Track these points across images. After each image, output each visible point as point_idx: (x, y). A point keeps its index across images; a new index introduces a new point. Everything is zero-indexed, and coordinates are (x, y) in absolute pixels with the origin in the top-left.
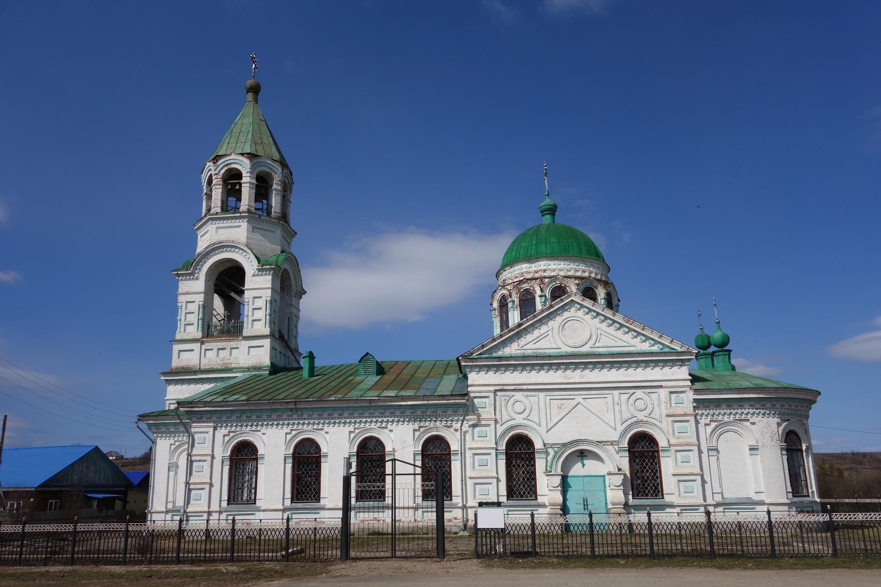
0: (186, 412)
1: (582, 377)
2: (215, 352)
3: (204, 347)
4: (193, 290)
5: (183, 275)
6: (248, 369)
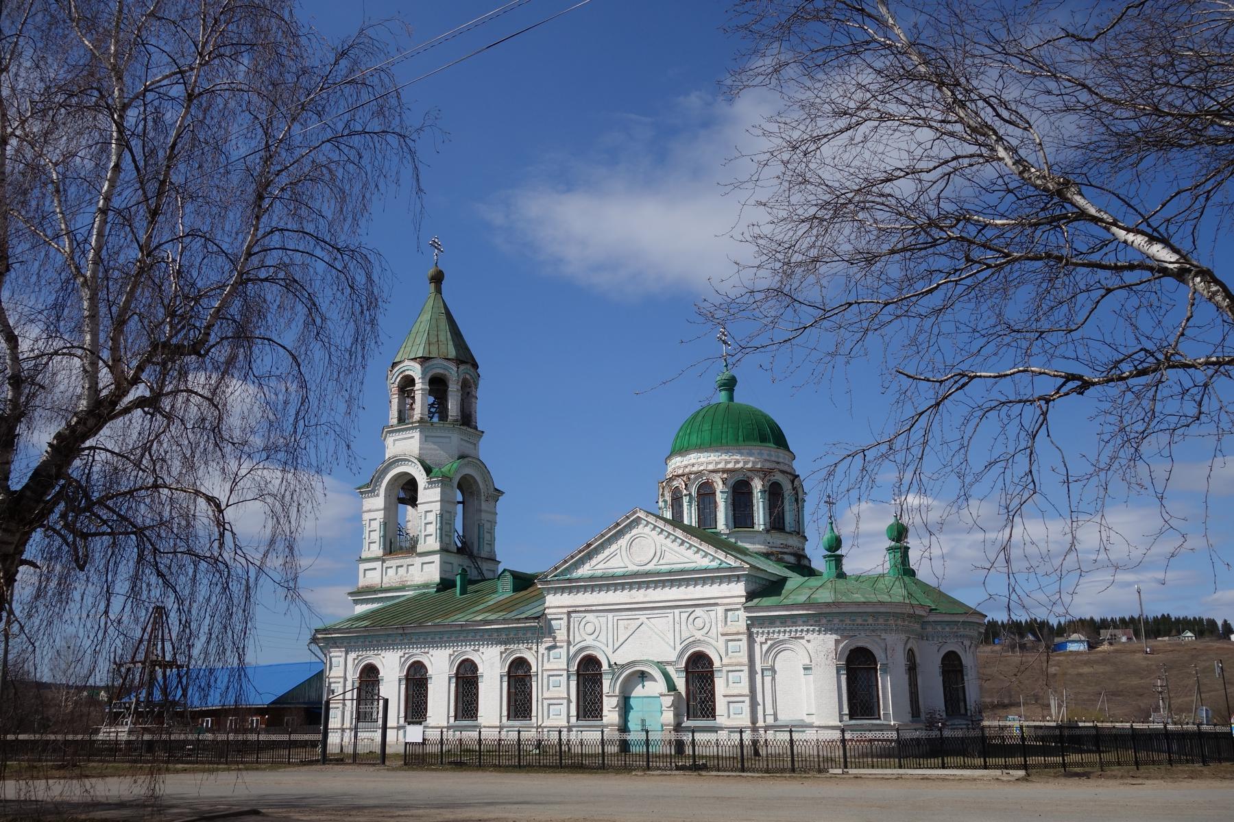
1: (645, 596)
6: (419, 587)
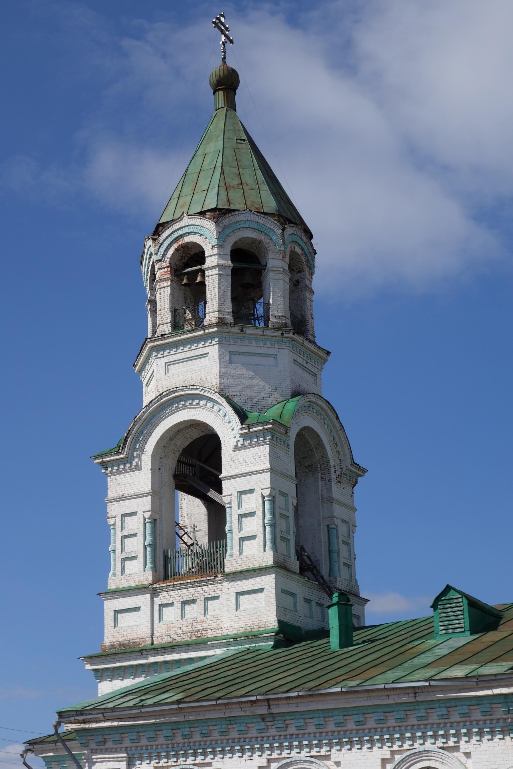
0: (77, 731)
2: (177, 609)
3: (157, 601)
4: (132, 490)
5: (112, 463)
6: (236, 639)
